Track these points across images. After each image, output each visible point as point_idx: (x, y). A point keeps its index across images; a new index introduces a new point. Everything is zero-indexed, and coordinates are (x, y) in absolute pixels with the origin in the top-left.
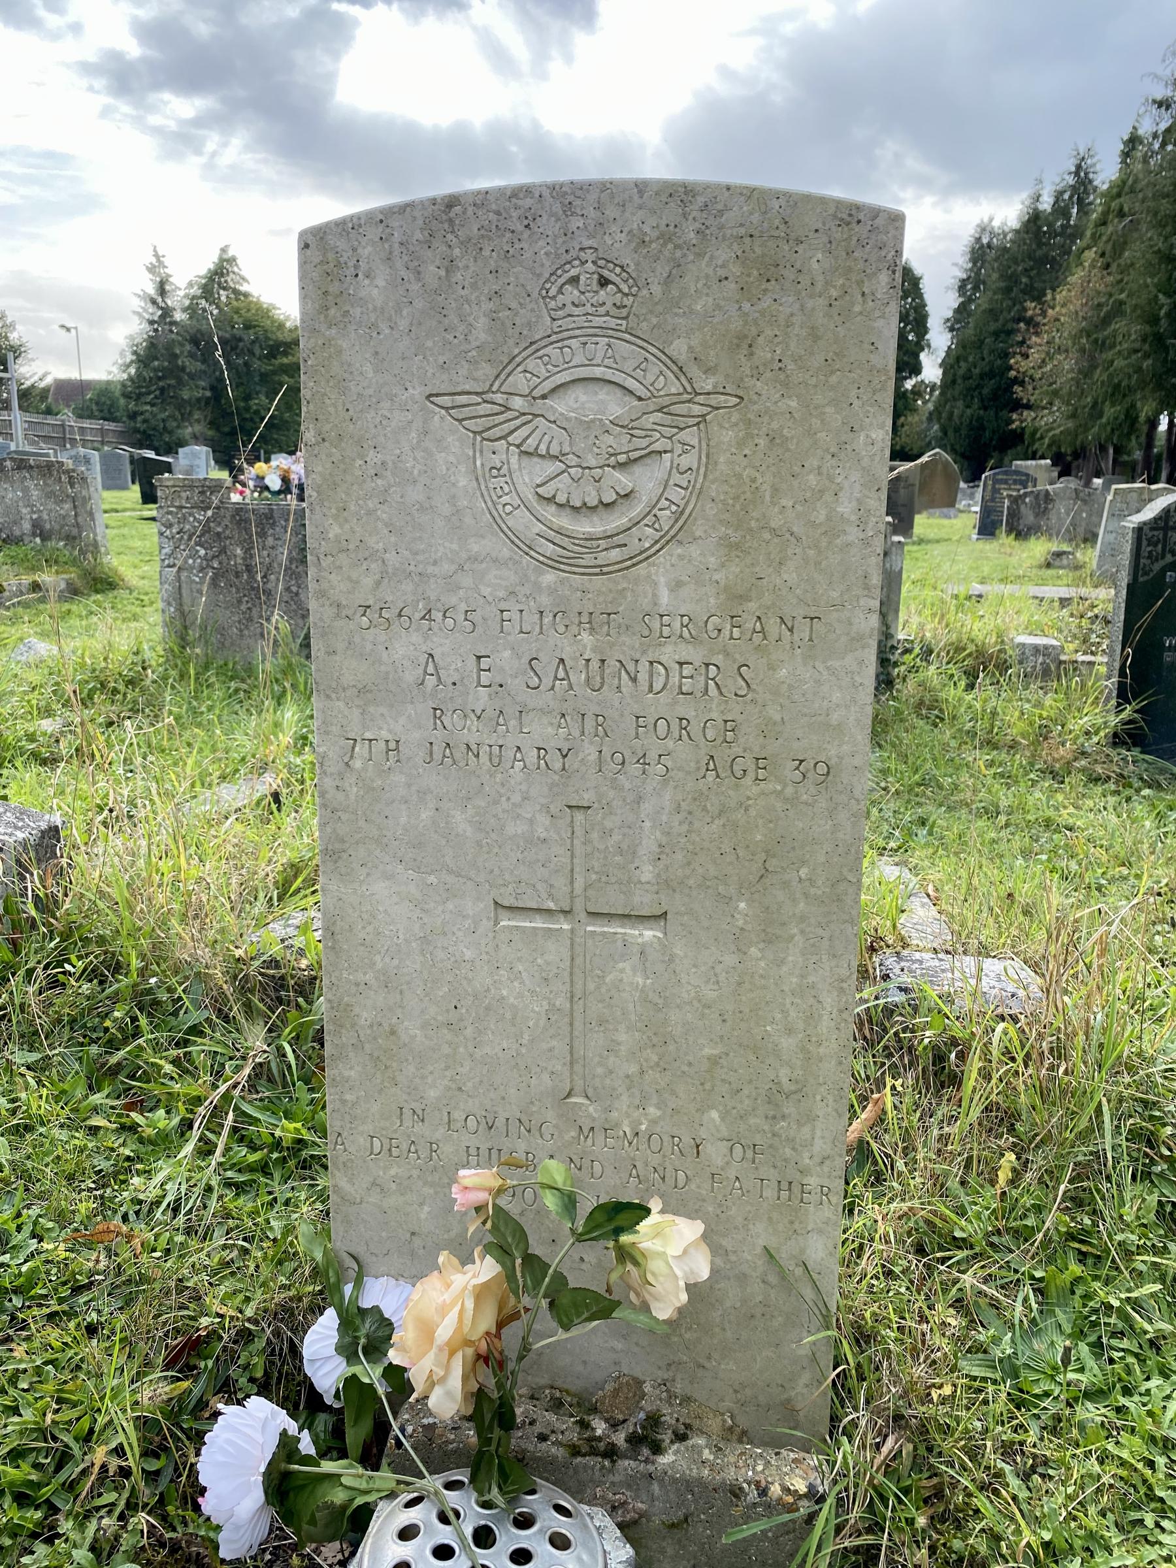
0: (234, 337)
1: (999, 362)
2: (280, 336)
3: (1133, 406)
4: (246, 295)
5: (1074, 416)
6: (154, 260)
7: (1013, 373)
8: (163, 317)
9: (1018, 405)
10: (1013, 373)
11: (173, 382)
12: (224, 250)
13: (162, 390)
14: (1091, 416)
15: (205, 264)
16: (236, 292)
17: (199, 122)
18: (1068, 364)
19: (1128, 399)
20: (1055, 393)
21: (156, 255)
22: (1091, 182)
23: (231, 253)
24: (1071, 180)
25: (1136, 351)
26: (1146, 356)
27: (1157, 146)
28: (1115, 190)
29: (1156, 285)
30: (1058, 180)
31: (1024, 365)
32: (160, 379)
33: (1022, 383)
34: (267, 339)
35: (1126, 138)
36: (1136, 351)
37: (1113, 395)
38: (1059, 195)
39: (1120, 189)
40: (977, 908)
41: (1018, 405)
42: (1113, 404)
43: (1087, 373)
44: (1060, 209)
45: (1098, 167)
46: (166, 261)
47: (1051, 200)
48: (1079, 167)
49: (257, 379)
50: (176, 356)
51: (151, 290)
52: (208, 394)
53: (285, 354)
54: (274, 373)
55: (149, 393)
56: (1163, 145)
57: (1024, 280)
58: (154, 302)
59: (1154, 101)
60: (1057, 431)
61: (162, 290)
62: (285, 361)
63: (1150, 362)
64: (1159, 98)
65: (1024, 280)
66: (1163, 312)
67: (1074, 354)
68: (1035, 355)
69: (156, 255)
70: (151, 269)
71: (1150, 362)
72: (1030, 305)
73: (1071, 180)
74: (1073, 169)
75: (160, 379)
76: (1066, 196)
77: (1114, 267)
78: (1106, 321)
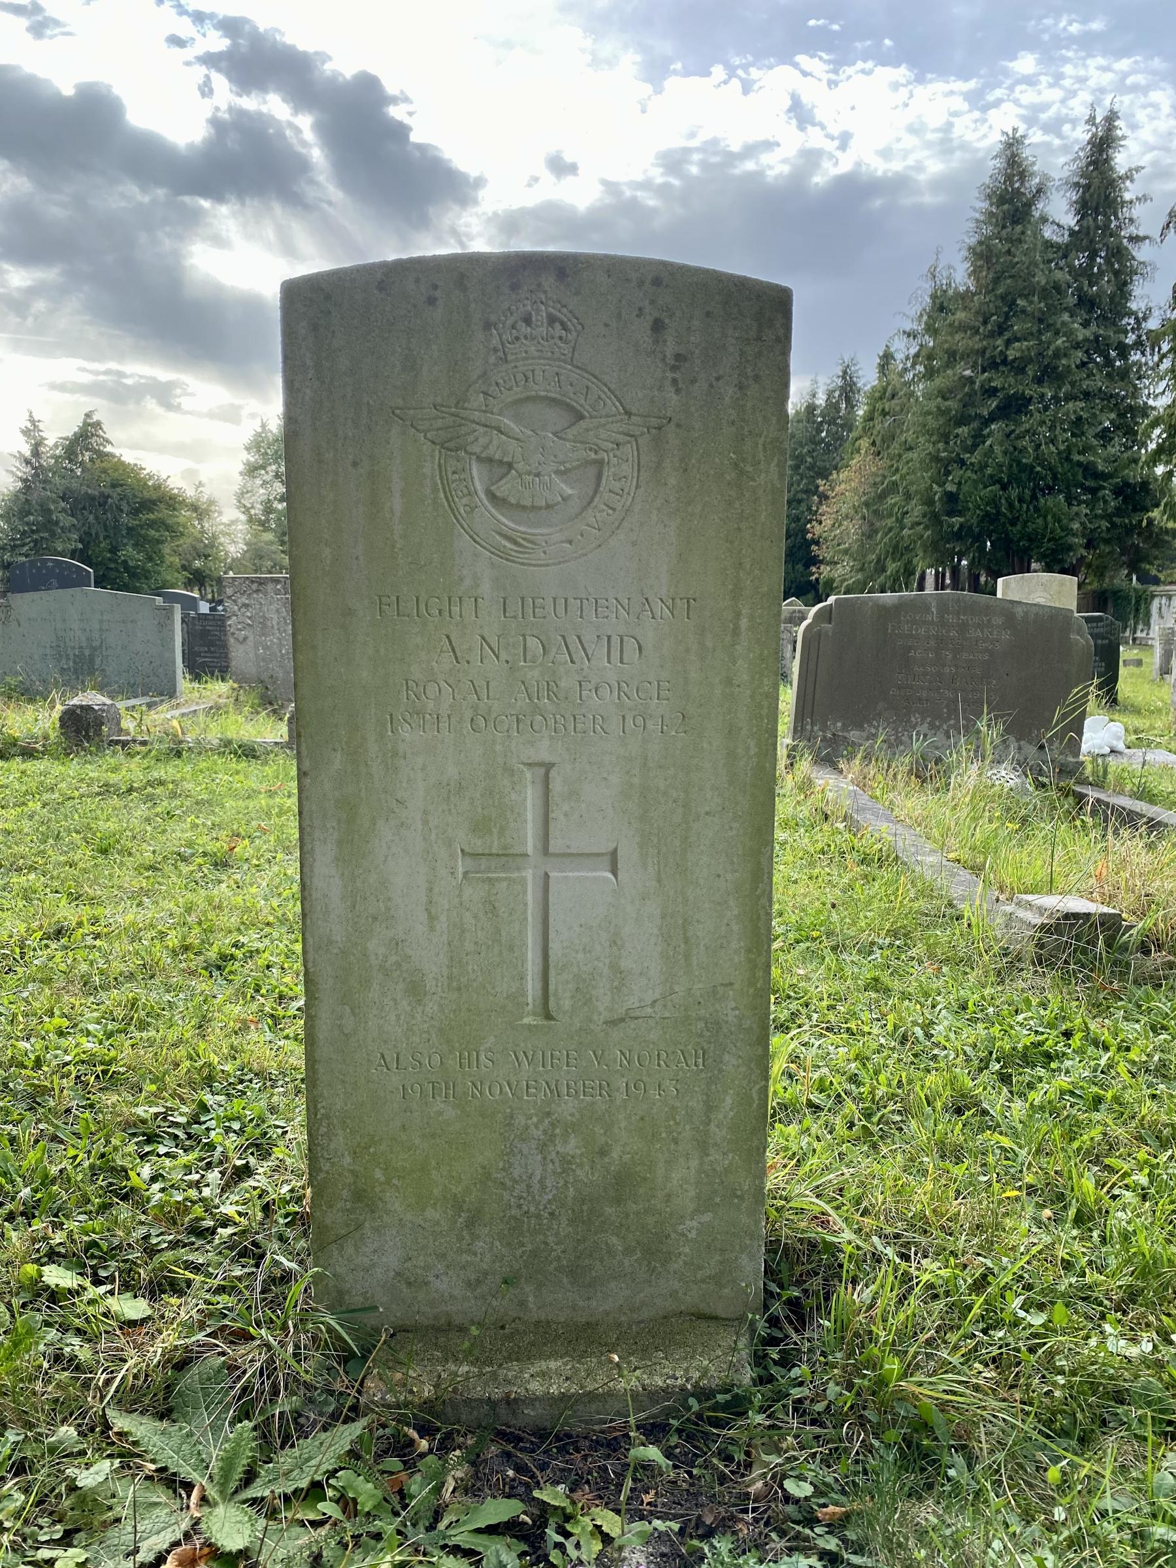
0: (102, 494)
1: (793, 525)
2: (146, 495)
3: (910, 562)
4: (108, 454)
5: (862, 569)
6: (29, 425)
7: (809, 536)
8: (36, 475)
9: (815, 561)
10: (809, 536)
11: (46, 535)
12: (88, 415)
13: (36, 541)
14: (876, 570)
15: (70, 429)
16: (102, 455)
17: (33, 292)
18: (852, 530)
19: (906, 557)
20: (846, 552)
21: (33, 422)
22: (855, 384)
23: (95, 418)
24: (840, 382)
25: (919, 524)
26: (926, 528)
27: (909, 365)
28: (877, 395)
29: (930, 478)
30: (829, 381)
31: (818, 529)
32: (33, 531)
33: (817, 543)
34: (135, 496)
35: (881, 354)
36: (919, 524)
37: (893, 553)
38: (830, 394)
39: (883, 394)
40: (1040, 1029)
41: (815, 561)
42: (894, 561)
43: (871, 534)
44: (832, 406)
45: (860, 373)
46: (41, 426)
47: (825, 397)
48: (845, 372)
49: (124, 532)
50: (49, 511)
51: (27, 451)
52: (80, 546)
53: (151, 511)
54: (141, 527)
55: (24, 545)
56: (914, 365)
57: (809, 460)
58: (28, 462)
59: (904, 332)
60: (851, 582)
61: (36, 453)
62: (151, 516)
63: (929, 532)
64: (908, 329)
65: (809, 460)
66: (937, 498)
67: (858, 522)
68: (828, 522)
69: (33, 422)
70: (26, 432)
71: (929, 532)
72: (820, 482)
73: (840, 382)
74: (841, 374)
75: (33, 531)
76: (837, 394)
77: (885, 454)
78: (882, 497)
